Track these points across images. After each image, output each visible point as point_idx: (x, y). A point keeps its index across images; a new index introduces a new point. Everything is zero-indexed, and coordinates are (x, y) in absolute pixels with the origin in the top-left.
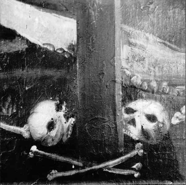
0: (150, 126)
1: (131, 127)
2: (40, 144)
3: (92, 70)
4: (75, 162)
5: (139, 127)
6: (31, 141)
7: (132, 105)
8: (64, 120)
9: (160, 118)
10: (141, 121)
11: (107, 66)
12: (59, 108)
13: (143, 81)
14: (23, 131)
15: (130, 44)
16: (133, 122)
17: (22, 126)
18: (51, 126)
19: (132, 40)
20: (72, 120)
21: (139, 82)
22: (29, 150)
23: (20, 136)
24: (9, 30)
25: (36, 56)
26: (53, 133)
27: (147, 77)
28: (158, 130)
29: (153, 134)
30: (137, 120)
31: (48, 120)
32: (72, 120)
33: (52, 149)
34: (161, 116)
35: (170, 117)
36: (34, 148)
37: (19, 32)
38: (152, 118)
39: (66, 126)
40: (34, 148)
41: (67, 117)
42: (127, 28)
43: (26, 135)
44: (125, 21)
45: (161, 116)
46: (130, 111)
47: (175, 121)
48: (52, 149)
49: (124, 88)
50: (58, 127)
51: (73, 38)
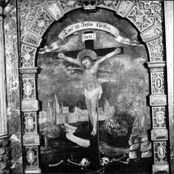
0: (106, 163)
1: (102, 163)
2: (83, 167)
3: (143, 97)
4: (90, 171)
5: (104, 163)
6: (81, 166)
7: (102, 159)
8: (88, 162)
9: (108, 161)
10: (104, 162)
11: (124, 100)
12: (87, 160)
13: (104, 153)
14: (80, 165)
15: (101, 145)
16: (102, 162)
17: (79, 164)
18: (85, 163)
19: (102, 145)
20: (90, 162)
21: (104, 153)
22: (81, 169)
23: (79, 166)
24: (76, 143)
25: (16, 165)
26: (86, 165)
27: (105, 152)
28: (108, 164)
29: (107, 165)
30: (103, 162)
31: (85, 162)
32: (90, 162)
33: (86, 168)
34: (108, 161)
35: (110, 160)
36: (82, 168)
37: (78, 144)
38: (106, 161)
39: (88, 163)
40: (82, 168)
41: (88, 161)
42: (100, 142)
43: (80, 165)
44: (100, 140)
45: (108, 161)
46: (102, 160)
47: (111, 162)
48: (86, 168)
49: (100, 155)
50: (87, 164)
51: (89, 144)
